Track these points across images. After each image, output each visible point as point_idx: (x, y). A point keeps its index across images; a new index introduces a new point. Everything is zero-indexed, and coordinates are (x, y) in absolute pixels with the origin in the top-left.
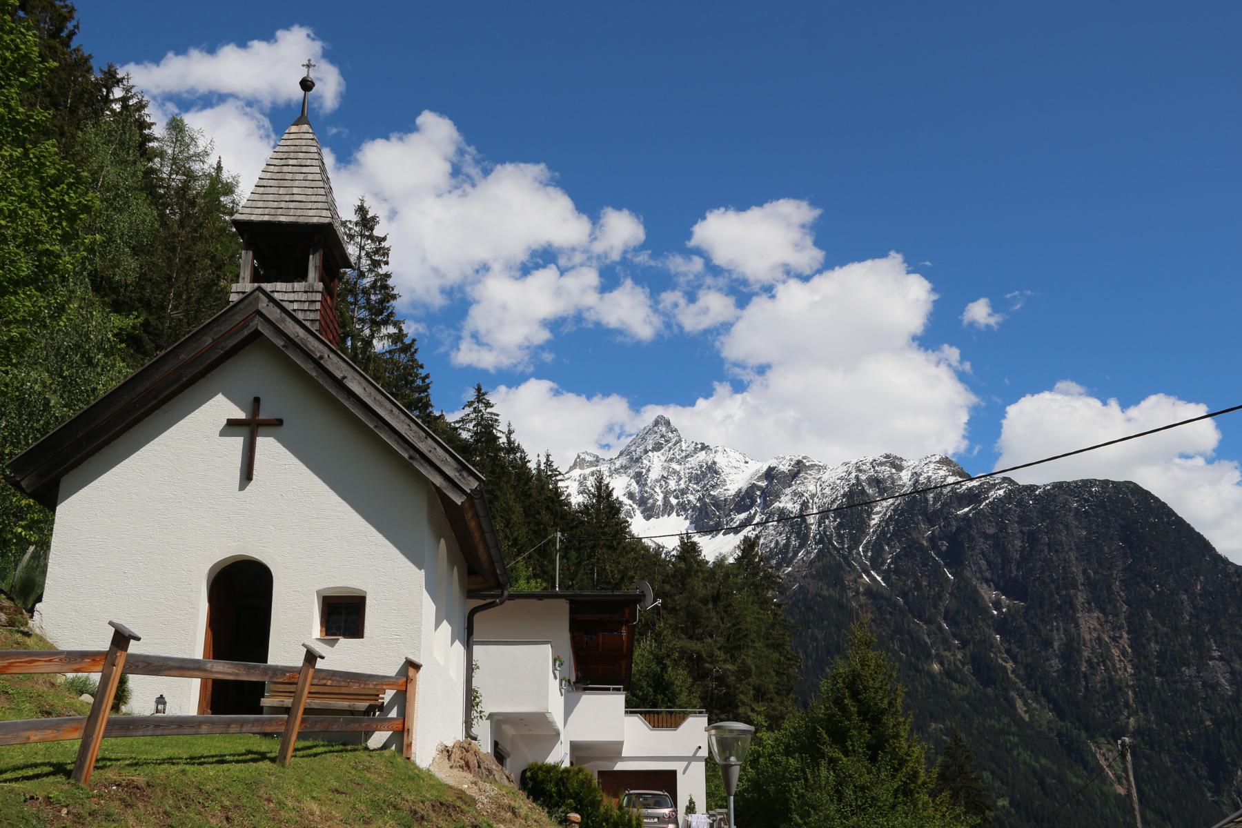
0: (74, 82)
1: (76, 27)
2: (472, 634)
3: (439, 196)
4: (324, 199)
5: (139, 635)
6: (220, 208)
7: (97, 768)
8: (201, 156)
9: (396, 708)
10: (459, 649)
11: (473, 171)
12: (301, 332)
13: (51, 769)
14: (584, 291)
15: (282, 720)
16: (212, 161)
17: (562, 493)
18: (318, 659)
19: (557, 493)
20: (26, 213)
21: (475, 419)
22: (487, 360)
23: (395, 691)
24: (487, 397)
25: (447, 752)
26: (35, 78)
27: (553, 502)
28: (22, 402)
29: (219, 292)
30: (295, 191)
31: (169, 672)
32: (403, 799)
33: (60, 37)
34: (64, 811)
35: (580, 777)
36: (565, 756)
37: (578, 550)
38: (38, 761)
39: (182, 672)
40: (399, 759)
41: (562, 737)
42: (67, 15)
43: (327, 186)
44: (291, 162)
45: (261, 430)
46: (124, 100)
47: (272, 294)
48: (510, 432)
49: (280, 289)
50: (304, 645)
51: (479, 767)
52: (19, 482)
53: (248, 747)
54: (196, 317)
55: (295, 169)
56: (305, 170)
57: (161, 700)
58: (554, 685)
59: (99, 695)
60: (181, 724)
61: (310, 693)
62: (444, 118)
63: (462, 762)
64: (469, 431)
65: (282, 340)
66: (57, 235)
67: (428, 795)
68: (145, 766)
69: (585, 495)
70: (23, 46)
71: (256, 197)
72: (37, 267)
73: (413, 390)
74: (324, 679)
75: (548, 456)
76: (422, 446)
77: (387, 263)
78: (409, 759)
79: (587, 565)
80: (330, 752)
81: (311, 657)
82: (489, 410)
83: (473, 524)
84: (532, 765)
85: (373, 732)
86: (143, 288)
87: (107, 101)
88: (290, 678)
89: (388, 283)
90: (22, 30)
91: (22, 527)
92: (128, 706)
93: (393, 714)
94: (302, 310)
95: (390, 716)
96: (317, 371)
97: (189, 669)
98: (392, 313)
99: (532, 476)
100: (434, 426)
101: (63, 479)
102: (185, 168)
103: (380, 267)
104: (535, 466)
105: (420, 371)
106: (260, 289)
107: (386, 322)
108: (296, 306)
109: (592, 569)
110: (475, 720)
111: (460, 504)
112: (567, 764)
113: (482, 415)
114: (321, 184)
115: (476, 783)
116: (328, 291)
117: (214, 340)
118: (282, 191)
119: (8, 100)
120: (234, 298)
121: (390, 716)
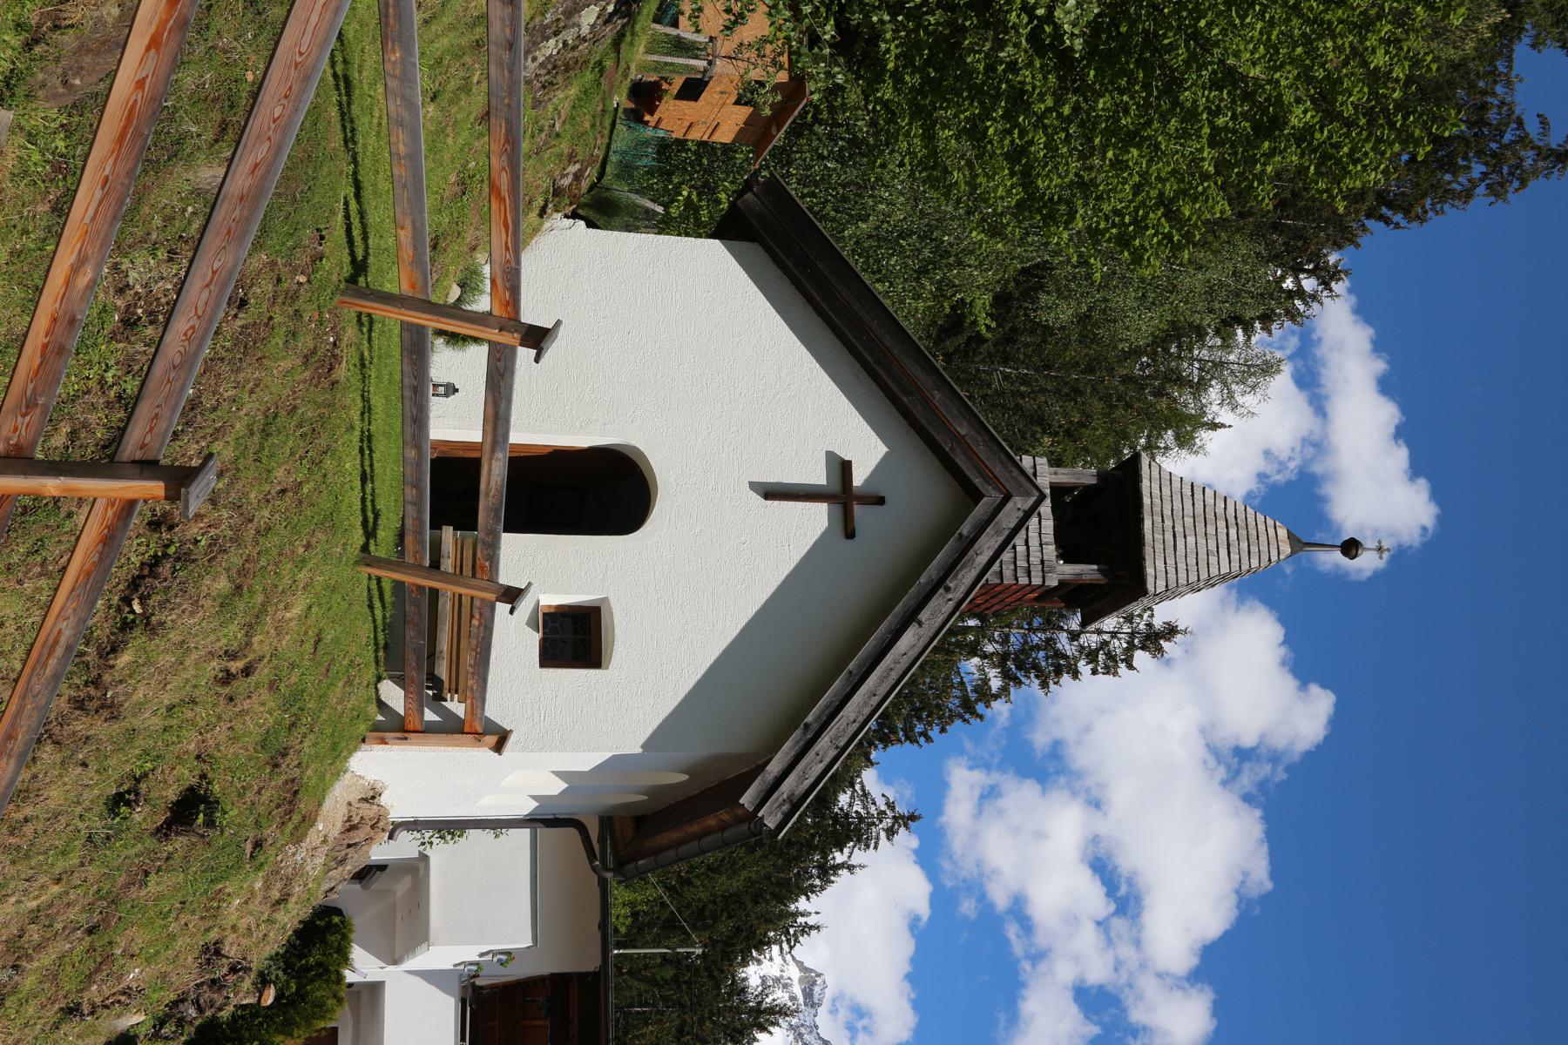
0: (1318, 226)
1: (1397, 226)
2: (547, 826)
3: (1203, 731)
4: (1183, 581)
5: (542, 361)
6: (1158, 429)
7: (359, 316)
8: (1229, 400)
9: (438, 719)
10: (525, 807)
11: (1246, 781)
12: (983, 559)
13: (360, 258)
14: (1076, 959)
15: (422, 558)
16: (1225, 416)
17: (761, 952)
18: (509, 606)
19: (762, 944)
20: (1125, 182)
21: (868, 813)
22: (958, 811)
23: (462, 716)
24: (902, 829)
25: (372, 797)
26: (1317, 184)
27: (747, 938)
28: (862, 187)
29: (1033, 436)
30: (1191, 540)
31: (490, 402)
32: (304, 736)
33: (1379, 206)
34: (302, 279)
35: (330, 1001)
36: (361, 974)
37: (676, 980)
38: (370, 241)
39: (491, 420)
40: (363, 727)
41: (391, 968)
42: (1413, 214)
43: (1201, 585)
44: (1233, 532)
45: (838, 508)
46: (1300, 293)
47: (1036, 514)
48: (851, 868)
49: (1045, 524)
50: (530, 584)
51: (349, 846)
52: (750, 189)
53: (384, 511)
54: (994, 406)
55: (1222, 538)
56: (1223, 552)
57: (451, 390)
58: (471, 953)
59: (455, 311)
60: (418, 419)
61: (460, 596)
62: (1326, 727)
63: (356, 820)
64: (851, 805)
65: (970, 532)
66: (1098, 223)
67: (309, 772)
68: (360, 377)
69: (760, 989)
70: (1359, 168)
71: (1176, 484)
72: (1051, 199)
73: (907, 720)
74: (481, 614)
75: (818, 928)
76: (824, 741)
77: (1094, 672)
78: (363, 741)
79: (654, 996)
80: (375, 627)
81: (512, 596)
82: (883, 835)
83: (712, 822)
84: (350, 924)
85: (403, 687)
86: (1032, 332)
87: (1297, 270)
88: (483, 568)
89: (1065, 675)
90: (1382, 166)
91: (689, 196)
92: (443, 347)
93: (430, 716)
94: (1015, 558)
95: (427, 711)
96: (925, 584)
97: (495, 429)
98: (1021, 683)
99: (785, 905)
100: (857, 754)
101: (756, 246)
102: (1210, 380)
103: (1088, 663)
104: (801, 909)
105: (936, 729)
106: (1042, 497)
107: (1006, 675)
108: (1021, 549)
109: (646, 1004)
110: (419, 836)
111: (741, 801)
112: (350, 977)
113: (874, 824)
114: (1204, 576)
115: (325, 842)
116: (1046, 594)
117: (963, 437)
118: (1189, 521)
119: (1281, 152)
120: (1027, 461)
121: (427, 711)
